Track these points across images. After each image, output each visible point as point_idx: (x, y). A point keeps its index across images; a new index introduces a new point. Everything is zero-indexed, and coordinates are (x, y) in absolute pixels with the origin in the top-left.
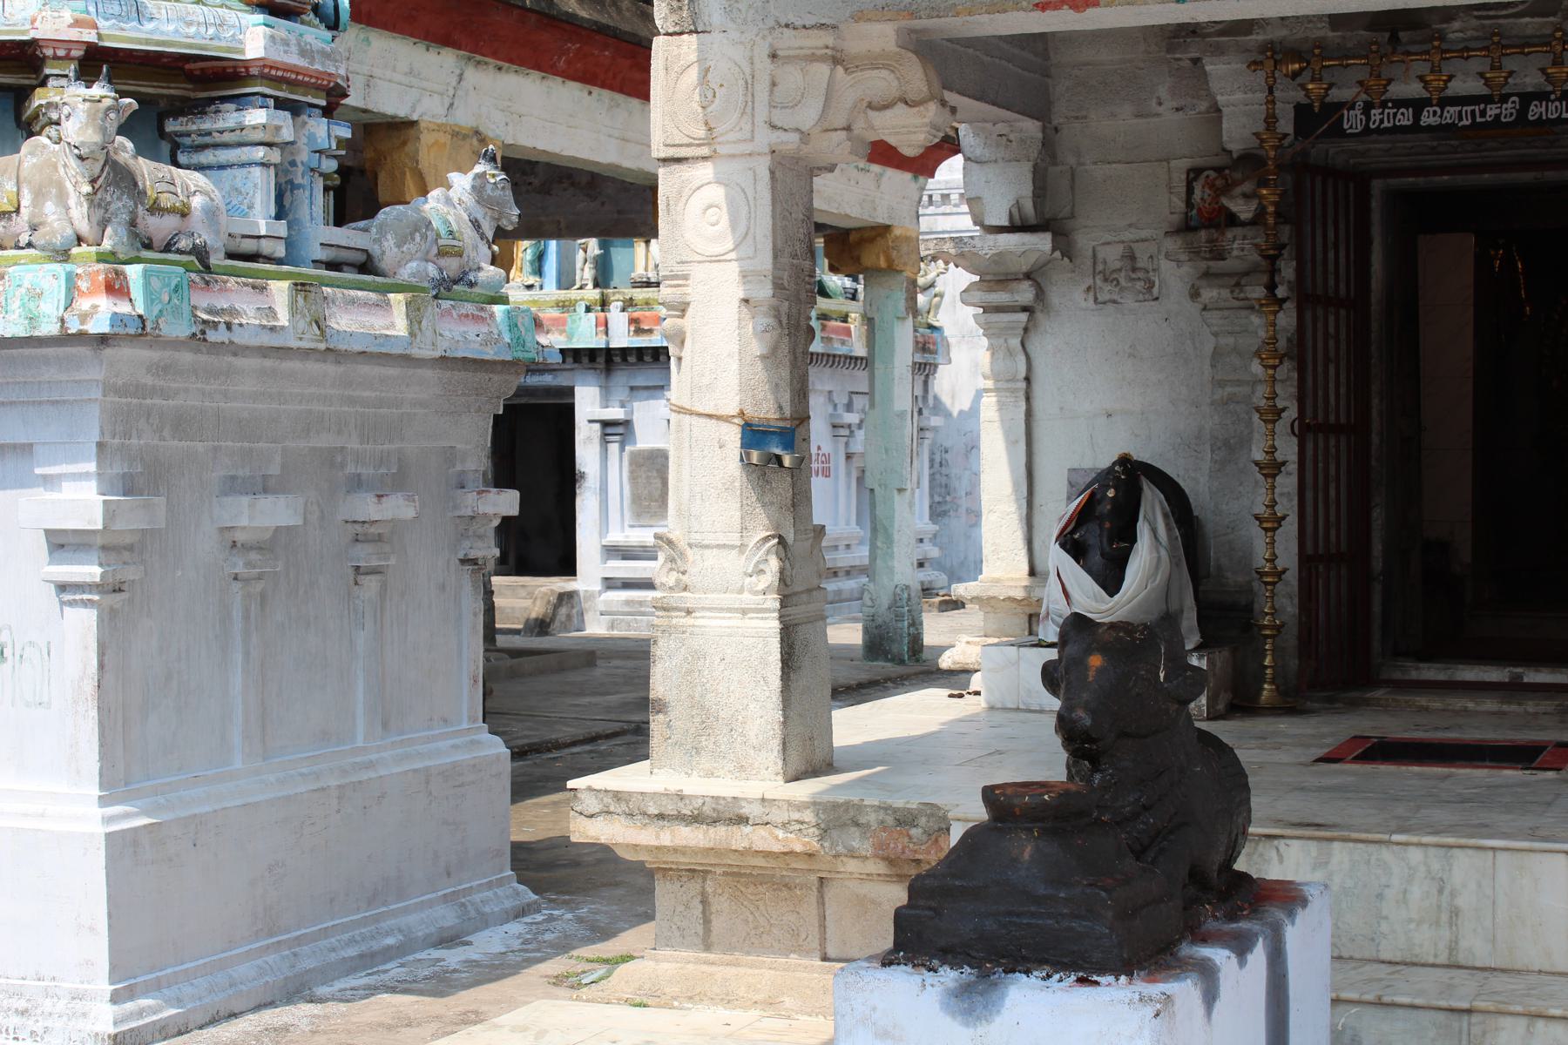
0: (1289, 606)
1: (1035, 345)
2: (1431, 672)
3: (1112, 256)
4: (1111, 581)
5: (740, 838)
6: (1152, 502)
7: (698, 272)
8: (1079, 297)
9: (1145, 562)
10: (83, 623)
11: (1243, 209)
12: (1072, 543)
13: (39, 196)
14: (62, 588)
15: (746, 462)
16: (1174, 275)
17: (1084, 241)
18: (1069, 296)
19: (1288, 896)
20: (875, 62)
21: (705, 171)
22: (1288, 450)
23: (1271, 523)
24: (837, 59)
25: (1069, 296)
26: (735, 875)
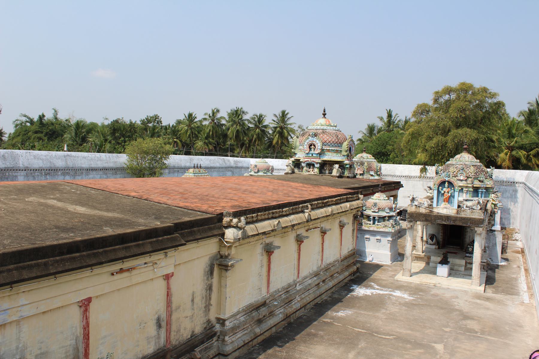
9: (434, 240)
10: (389, 244)
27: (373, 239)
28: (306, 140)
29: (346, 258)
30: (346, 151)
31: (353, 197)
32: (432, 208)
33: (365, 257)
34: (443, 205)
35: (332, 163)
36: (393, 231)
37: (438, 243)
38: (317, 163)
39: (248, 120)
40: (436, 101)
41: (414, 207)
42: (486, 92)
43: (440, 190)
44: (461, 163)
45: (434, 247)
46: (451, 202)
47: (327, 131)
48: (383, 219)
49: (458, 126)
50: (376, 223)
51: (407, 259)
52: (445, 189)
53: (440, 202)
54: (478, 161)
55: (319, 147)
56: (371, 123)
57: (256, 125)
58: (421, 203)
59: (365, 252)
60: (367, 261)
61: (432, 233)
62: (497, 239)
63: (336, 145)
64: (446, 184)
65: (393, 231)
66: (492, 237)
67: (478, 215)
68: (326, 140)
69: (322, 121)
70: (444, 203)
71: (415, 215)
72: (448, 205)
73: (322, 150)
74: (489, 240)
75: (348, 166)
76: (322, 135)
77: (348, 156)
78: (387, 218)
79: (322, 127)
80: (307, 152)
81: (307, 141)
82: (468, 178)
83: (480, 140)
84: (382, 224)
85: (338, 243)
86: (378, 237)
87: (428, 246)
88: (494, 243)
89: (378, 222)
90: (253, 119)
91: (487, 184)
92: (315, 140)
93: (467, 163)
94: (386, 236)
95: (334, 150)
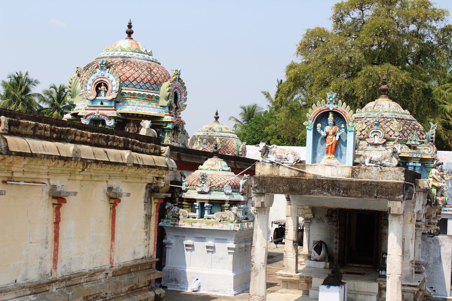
0: (337, 257)
1: (310, 227)
2: (351, 265)
3: (319, 217)
4: (319, 254)
5: (292, 278)
6: (323, 245)
7: (289, 227)
8: (315, 222)
9: (323, 252)
10: (231, 256)
11: (334, 216)
12: (315, 249)
13: (229, 217)
14: (229, 253)
15: (293, 245)
16: (326, 220)
17: (316, 216)
18: (314, 222)
19: (345, 283)
20: (307, 209)
21: (291, 218)
22: (338, 241)
23: (336, 249)
24: (303, 209)
25: (314, 222)
26: (290, 282)
27: (200, 246)
28: (91, 75)
29: (127, 270)
30: (168, 98)
31: (145, 146)
32: (304, 167)
33: (186, 283)
34: (325, 159)
35: (137, 119)
36: (238, 229)
37: (329, 258)
38: (110, 118)
39: (39, 95)
40: (338, 20)
41: (268, 166)
42: (426, 8)
43: (318, 129)
44: (376, 115)
45: (322, 265)
46: (341, 155)
47: (132, 60)
48: (218, 205)
49: (375, 59)
50: (206, 214)
51: (257, 274)
52: (327, 128)
53: (319, 155)
54: (407, 111)
55: (114, 88)
56: (248, 103)
57: (53, 105)
58: (281, 158)
59: (185, 273)
60: (189, 290)
61: (318, 239)
62: (442, 248)
63: (148, 85)
64: (331, 118)
65: (238, 229)
66: (432, 246)
67: (395, 176)
68: (128, 75)
69: (125, 43)
70: (326, 157)
71: (269, 181)
72: (334, 161)
73: (120, 94)
74: (428, 252)
75: (170, 126)
76: (120, 67)
77: (170, 107)
78: (227, 205)
79: (122, 54)
80: (92, 97)
81: (93, 77)
82: (388, 140)
83: (416, 89)
84: (218, 215)
85: (105, 234)
86: (210, 243)
87: (312, 263)
88: (437, 257)
89: (211, 213)
90: (49, 93)
91: (424, 153)
92: (107, 75)
93: (386, 115)
94: (224, 241)
95: (143, 95)
